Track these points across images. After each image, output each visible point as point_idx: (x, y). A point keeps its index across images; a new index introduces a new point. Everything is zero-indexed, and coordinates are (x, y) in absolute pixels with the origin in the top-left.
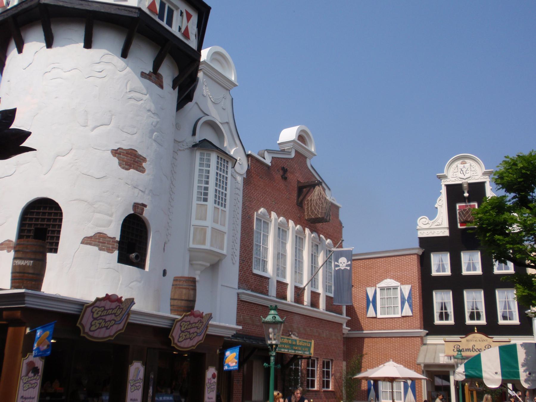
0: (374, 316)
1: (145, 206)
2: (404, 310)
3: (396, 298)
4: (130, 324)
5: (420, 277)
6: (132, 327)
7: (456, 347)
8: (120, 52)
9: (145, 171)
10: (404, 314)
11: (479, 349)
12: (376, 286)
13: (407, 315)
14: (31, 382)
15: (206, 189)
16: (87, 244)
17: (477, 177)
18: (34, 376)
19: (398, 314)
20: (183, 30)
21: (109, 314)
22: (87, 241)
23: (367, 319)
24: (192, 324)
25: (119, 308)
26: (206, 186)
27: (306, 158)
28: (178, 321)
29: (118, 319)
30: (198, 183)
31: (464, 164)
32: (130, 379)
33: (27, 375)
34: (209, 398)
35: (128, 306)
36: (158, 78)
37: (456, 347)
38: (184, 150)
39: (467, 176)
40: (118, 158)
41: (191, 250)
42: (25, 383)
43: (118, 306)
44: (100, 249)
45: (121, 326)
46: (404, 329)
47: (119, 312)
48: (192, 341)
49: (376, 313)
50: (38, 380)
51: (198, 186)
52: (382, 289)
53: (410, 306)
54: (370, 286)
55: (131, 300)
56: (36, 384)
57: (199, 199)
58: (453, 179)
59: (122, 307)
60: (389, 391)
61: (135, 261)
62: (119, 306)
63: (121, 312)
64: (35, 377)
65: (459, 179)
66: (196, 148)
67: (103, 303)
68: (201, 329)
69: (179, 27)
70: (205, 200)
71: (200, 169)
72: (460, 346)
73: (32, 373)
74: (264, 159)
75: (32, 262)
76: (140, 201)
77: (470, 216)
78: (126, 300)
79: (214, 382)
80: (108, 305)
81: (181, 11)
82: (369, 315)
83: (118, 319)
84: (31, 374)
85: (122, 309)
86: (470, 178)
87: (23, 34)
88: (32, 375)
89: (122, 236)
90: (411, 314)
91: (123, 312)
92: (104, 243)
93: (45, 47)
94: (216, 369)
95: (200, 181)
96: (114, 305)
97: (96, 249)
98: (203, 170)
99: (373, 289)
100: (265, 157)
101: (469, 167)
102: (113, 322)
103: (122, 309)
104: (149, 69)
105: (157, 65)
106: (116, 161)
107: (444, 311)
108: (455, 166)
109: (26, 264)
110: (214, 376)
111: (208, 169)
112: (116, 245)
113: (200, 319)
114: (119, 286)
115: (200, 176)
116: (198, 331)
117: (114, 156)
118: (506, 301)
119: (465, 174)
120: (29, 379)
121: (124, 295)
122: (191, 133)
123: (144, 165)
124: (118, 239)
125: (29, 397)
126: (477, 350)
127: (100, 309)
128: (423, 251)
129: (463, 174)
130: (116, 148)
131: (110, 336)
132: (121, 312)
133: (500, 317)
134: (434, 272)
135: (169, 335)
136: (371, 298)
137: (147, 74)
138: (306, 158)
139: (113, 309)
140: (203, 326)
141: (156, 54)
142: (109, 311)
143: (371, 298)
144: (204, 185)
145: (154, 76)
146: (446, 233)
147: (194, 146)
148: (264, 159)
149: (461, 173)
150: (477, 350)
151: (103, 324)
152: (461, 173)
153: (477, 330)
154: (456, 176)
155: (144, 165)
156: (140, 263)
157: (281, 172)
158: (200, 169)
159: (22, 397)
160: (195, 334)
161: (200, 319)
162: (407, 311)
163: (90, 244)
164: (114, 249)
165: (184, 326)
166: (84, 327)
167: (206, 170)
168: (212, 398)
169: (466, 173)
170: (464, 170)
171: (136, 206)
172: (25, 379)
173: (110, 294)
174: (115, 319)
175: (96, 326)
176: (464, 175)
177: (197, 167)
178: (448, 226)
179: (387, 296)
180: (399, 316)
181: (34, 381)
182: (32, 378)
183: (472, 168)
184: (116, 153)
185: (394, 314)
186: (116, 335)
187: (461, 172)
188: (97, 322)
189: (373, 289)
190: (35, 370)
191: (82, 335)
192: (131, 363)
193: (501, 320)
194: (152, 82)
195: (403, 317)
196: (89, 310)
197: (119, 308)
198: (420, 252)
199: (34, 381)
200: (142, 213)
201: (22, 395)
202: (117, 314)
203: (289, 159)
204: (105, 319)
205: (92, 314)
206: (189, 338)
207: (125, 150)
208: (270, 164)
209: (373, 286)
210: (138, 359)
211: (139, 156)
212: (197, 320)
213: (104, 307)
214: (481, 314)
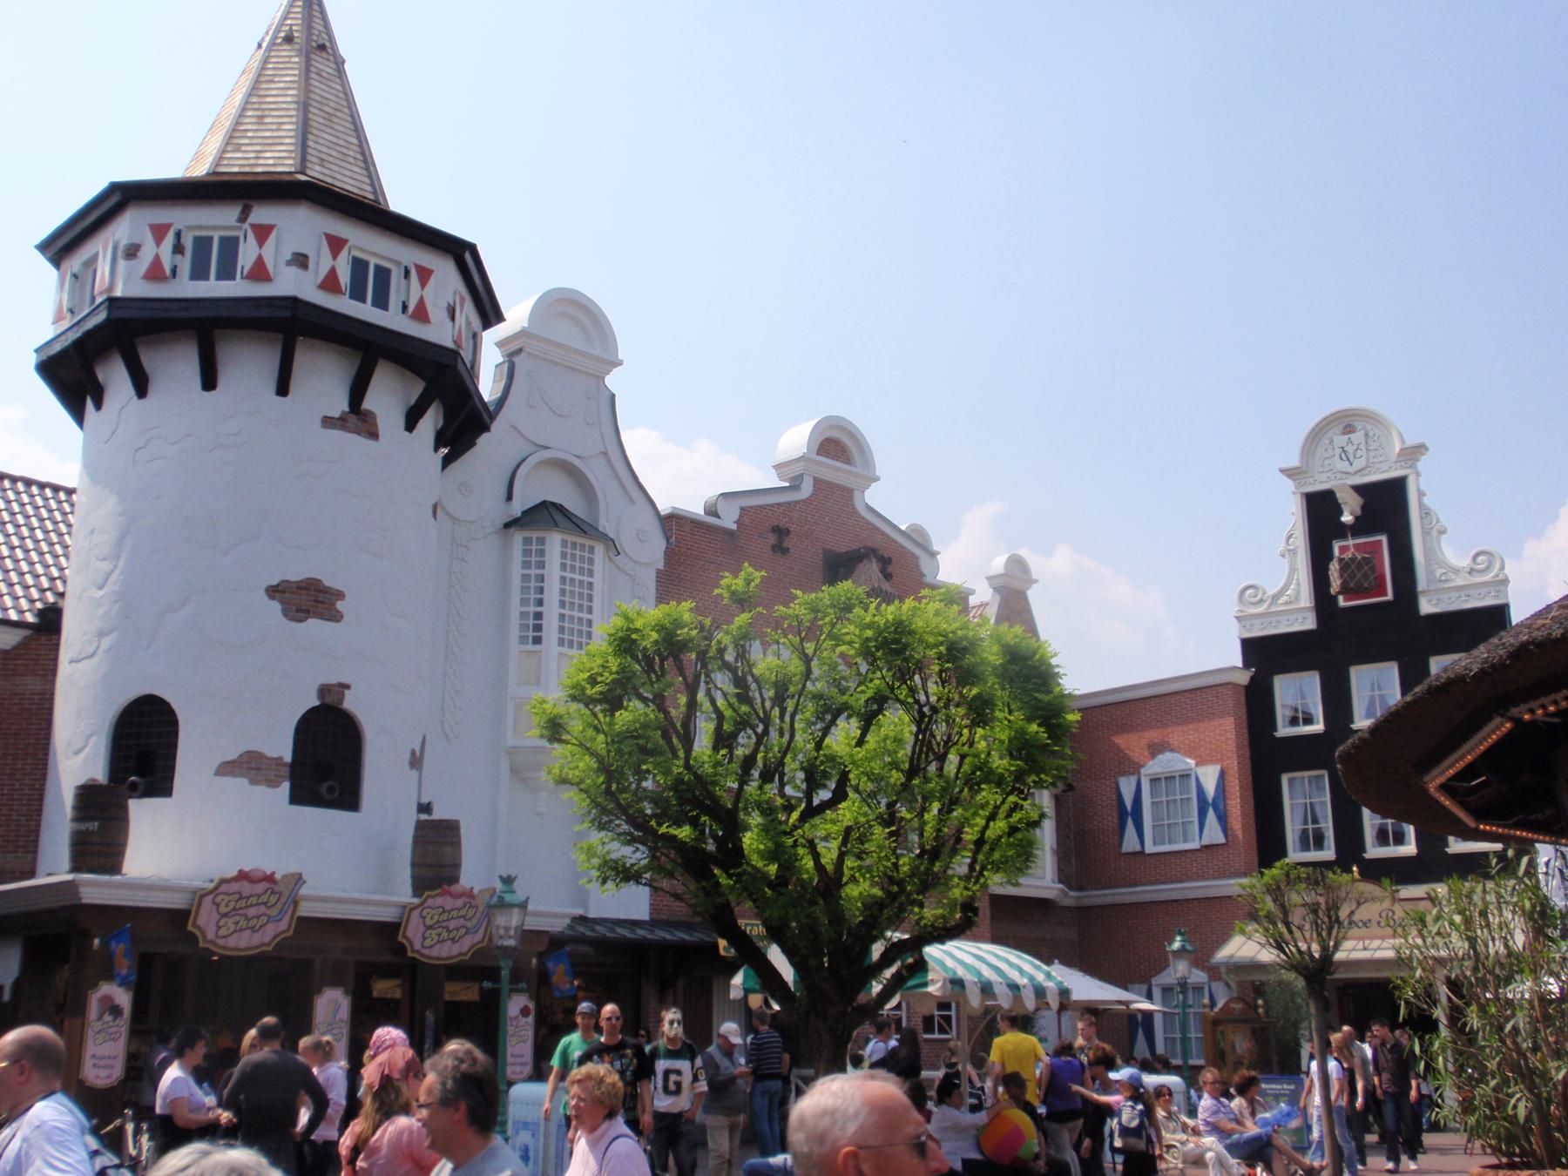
0: (1138, 848)
1: (347, 687)
2: (1206, 831)
3: (1188, 799)
4: (302, 920)
5: (1246, 743)
6: (308, 925)
7: (1384, 915)
8: (272, 386)
9: (342, 617)
10: (1206, 841)
11: (1364, 920)
12: (1139, 773)
13: (1215, 842)
14: (109, 1030)
15: (538, 616)
16: (224, 775)
17: (1384, 466)
18: (115, 1019)
19: (1194, 841)
20: (412, 306)
21: (252, 906)
22: (227, 768)
23: (1122, 859)
24: (449, 912)
25: (272, 893)
26: (539, 609)
27: (850, 491)
28: (412, 910)
29: (274, 912)
30: (521, 606)
31: (1350, 432)
32: (91, 1020)
33: (100, 1017)
34: (512, 1055)
35: (290, 888)
36: (364, 421)
37: (1384, 915)
38: (485, 537)
39: (1358, 464)
40: (281, 602)
41: (512, 751)
42: (98, 1033)
43: (267, 890)
44: (253, 782)
45: (283, 925)
46: (1208, 879)
47: (273, 899)
48: (457, 945)
49: (1142, 843)
50: (123, 1026)
51: (521, 613)
52: (1154, 781)
53: (1223, 819)
54: (1126, 773)
55: (297, 877)
56: (118, 1035)
57: (523, 640)
58: (1324, 477)
59: (277, 889)
60: (1197, 1038)
61: (328, 797)
62: (273, 889)
63: (279, 899)
64: (116, 1023)
65: (1339, 476)
66: (513, 530)
67: (235, 887)
68: (474, 921)
69: (404, 303)
70: (537, 640)
71: (523, 575)
72: (1394, 913)
73: (110, 1014)
74: (719, 517)
75: (96, 824)
76: (333, 680)
77: (1355, 575)
78: (285, 877)
79: (526, 1023)
80: (246, 888)
81: (406, 267)
82: (1124, 850)
83: (274, 912)
84: (108, 1018)
85: (280, 893)
86: (1366, 471)
87: (101, 376)
88: (110, 1018)
89: (296, 752)
90: (1222, 840)
91: (283, 900)
92: (259, 769)
93: (136, 398)
94: (531, 998)
95: (524, 602)
96: (260, 888)
97: (245, 781)
98: (529, 576)
99: (1133, 779)
100: (720, 513)
101: (1363, 440)
102: (266, 919)
103: (280, 893)
104: (339, 404)
105: (357, 393)
106: (276, 606)
107: (1310, 826)
108: (1327, 442)
109: (88, 829)
110: (525, 1012)
111: (539, 572)
112: (286, 771)
113: (467, 900)
114: (1416, 690)
115: (525, 589)
116: (469, 925)
117: (272, 597)
118: (1306, 804)
119: (1351, 459)
120: (105, 1026)
121: (279, 867)
122: (504, 494)
123: (340, 605)
124: (288, 758)
125: (107, 1054)
126: (1360, 924)
127: (231, 897)
128: (1252, 674)
129: (1348, 459)
130: (275, 583)
131: (262, 945)
132: (279, 899)
133: (1294, 842)
134: (1284, 727)
135: (397, 936)
136: (1129, 805)
137: (337, 419)
138: (850, 491)
139: (259, 896)
140: (478, 915)
141: (353, 372)
142: (251, 899)
143: (1129, 805)
144: (533, 609)
145: (353, 419)
146: (1308, 623)
147: (508, 525)
148: (719, 517)
149: (1341, 459)
150: (1360, 924)
151: (243, 923)
152: (1341, 459)
153: (1360, 873)
154: (1331, 467)
155: (340, 605)
156: (348, 797)
157: (772, 539)
158: (523, 575)
159: (93, 1056)
160: (463, 931)
161: (467, 900)
162: (1213, 833)
163: (233, 774)
164: (280, 779)
165: (429, 916)
166: (203, 933)
167: (537, 576)
168: (522, 1056)
169: (1355, 457)
170: (1350, 449)
171: (324, 690)
172: (97, 1026)
173: (247, 869)
174: (268, 912)
175: (228, 929)
176: (1351, 464)
177: (517, 570)
178: (1313, 605)
179: (1167, 796)
180: (1195, 845)
181: (114, 1029)
182: (111, 1024)
183: (1370, 441)
184: (274, 591)
185: (1185, 841)
186: (276, 941)
187: (1343, 455)
188: (230, 921)
189: (1133, 779)
190: (116, 1011)
191: (202, 944)
192: (319, 992)
193: (1374, 846)
194: (350, 432)
195: (1206, 846)
196: (208, 901)
197: (272, 893)
198: (1244, 678)
199: (114, 1029)
200: (341, 700)
201: (92, 1053)
202: (269, 904)
203: (796, 502)
204: (245, 915)
205: (215, 907)
206: (448, 939)
207: (295, 582)
208: (734, 527)
209: (1130, 774)
210: (334, 983)
211: (326, 591)
212: (459, 902)
213: (239, 893)
214: (1326, 835)
